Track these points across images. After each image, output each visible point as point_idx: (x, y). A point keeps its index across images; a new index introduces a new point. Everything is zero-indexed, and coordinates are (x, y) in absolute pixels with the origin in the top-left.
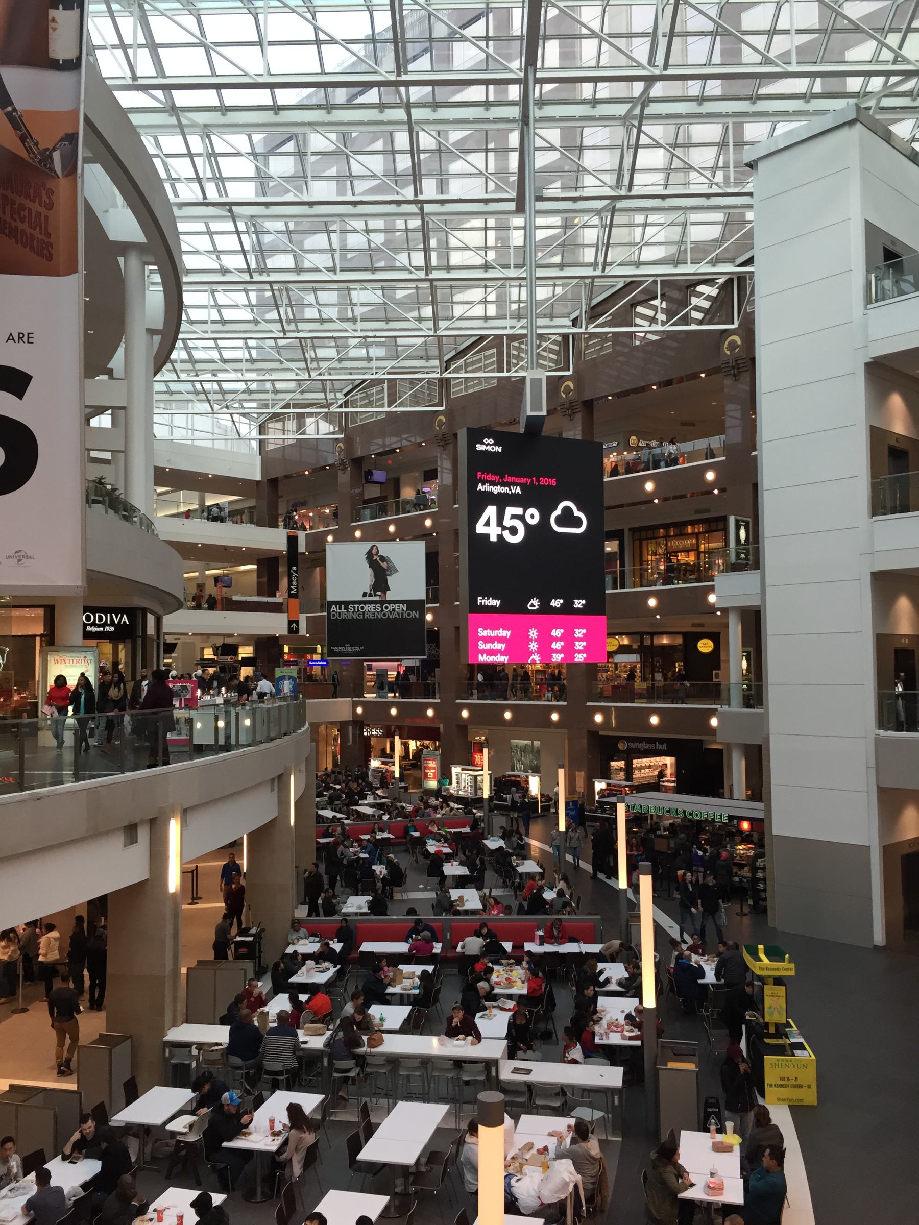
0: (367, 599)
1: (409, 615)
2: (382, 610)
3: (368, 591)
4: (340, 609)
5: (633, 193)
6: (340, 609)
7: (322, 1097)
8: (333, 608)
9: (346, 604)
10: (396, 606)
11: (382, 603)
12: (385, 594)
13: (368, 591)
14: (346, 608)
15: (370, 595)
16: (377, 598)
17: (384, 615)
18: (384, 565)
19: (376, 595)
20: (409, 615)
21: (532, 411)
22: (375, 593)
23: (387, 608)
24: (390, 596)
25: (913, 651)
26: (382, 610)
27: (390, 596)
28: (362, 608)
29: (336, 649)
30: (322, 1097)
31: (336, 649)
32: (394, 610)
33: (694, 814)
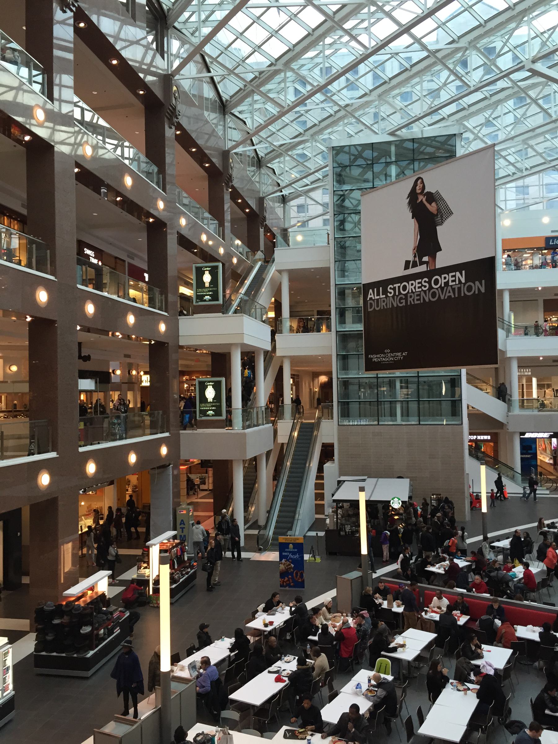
0: (412, 271)
1: (469, 289)
2: (431, 287)
3: (411, 258)
4: (378, 294)
5: (529, 156)
6: (378, 294)
7: (436, 635)
8: (371, 295)
9: (383, 285)
10: (449, 277)
11: (429, 274)
12: (434, 257)
13: (411, 258)
14: (385, 292)
15: (415, 265)
16: (423, 268)
17: (434, 295)
18: (432, 208)
19: (422, 263)
20: (469, 289)
21: (316, 636)
22: (420, 258)
23: (436, 282)
24: (442, 260)
25: (53, 322)
26: (431, 287)
27: (442, 260)
28: (405, 288)
29: (375, 358)
30: (436, 635)
31: (375, 358)
32: (447, 284)
33: (355, 218)
